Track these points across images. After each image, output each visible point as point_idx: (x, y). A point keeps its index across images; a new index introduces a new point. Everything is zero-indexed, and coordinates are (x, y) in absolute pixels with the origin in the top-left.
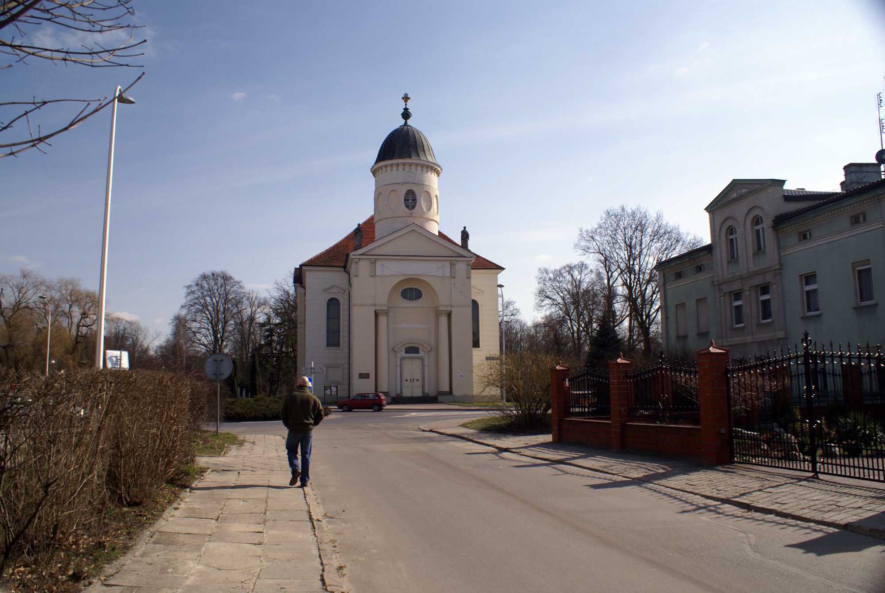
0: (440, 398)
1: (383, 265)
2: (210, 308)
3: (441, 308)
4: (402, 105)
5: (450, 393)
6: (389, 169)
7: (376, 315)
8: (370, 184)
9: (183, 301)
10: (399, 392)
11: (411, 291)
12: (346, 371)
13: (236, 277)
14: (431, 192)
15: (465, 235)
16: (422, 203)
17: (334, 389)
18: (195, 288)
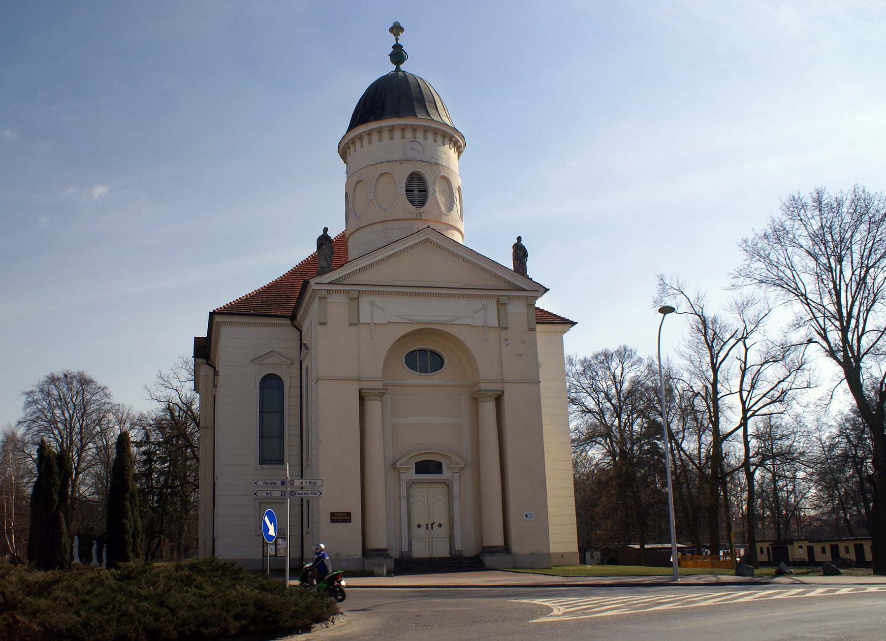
0: (488, 560)
1: (373, 304)
2: (60, 425)
3: (483, 386)
5: (506, 548)
6: (386, 135)
7: (362, 399)
8: (334, 179)
9: (20, 415)
10: (405, 549)
11: (423, 355)
13: (100, 381)
14: (451, 178)
15: (520, 253)
16: (438, 195)
18: (38, 396)
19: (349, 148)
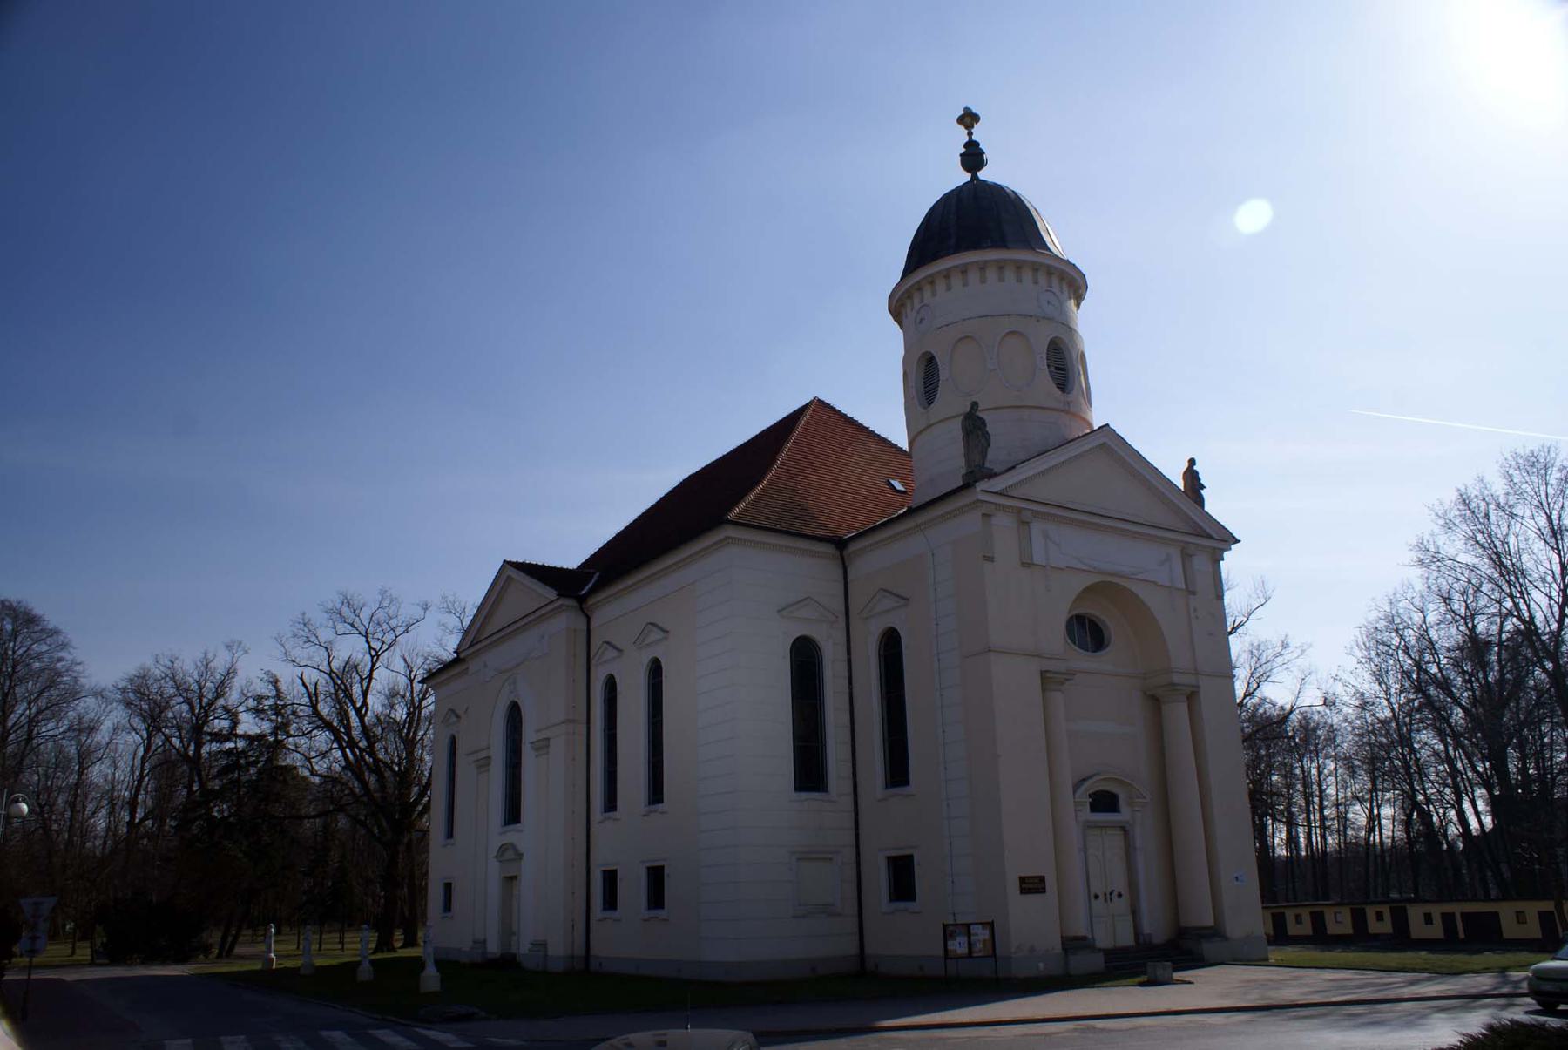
1: (1046, 536)
3: (1176, 678)
4: (962, 135)
6: (956, 281)
12: (851, 872)
13: (52, 619)
15: (1191, 475)
17: (980, 934)
19: (903, 305)
